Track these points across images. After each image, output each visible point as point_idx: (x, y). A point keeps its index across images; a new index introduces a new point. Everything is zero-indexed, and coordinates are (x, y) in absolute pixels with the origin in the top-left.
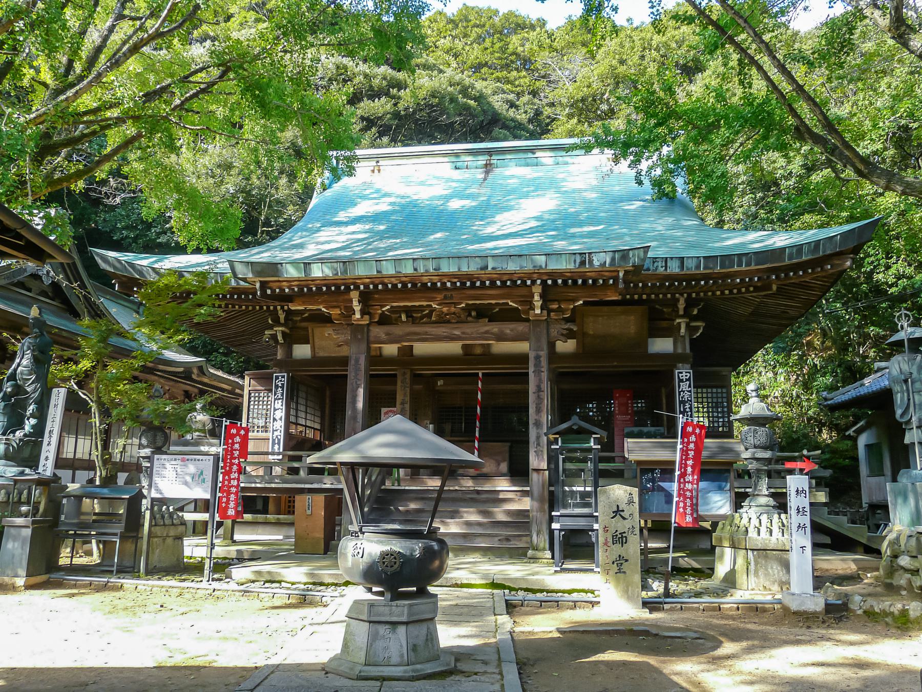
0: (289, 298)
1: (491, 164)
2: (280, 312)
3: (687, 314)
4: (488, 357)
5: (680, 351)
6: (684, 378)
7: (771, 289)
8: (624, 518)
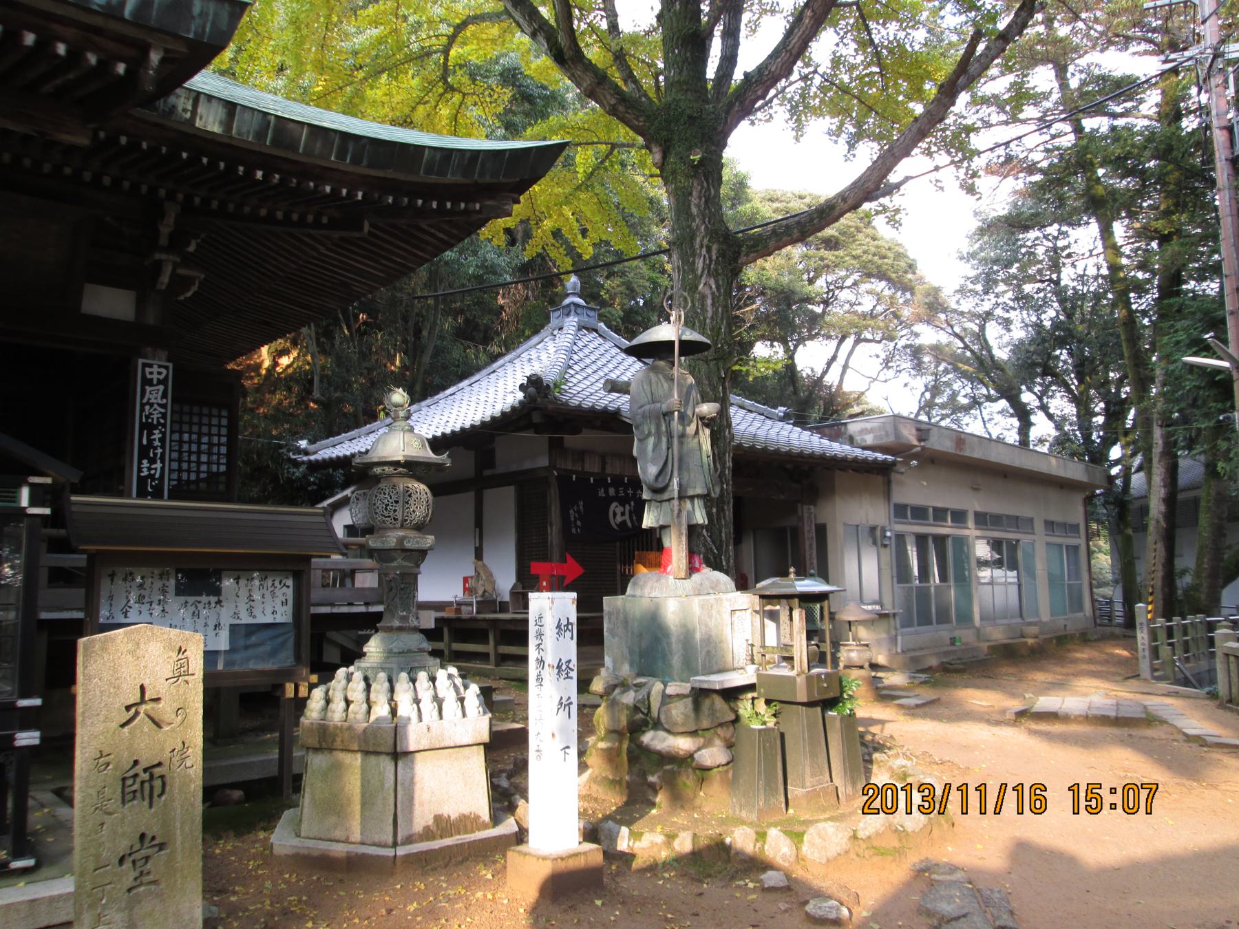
3: (177, 242)
5: (151, 318)
6: (155, 377)
7: (361, 229)
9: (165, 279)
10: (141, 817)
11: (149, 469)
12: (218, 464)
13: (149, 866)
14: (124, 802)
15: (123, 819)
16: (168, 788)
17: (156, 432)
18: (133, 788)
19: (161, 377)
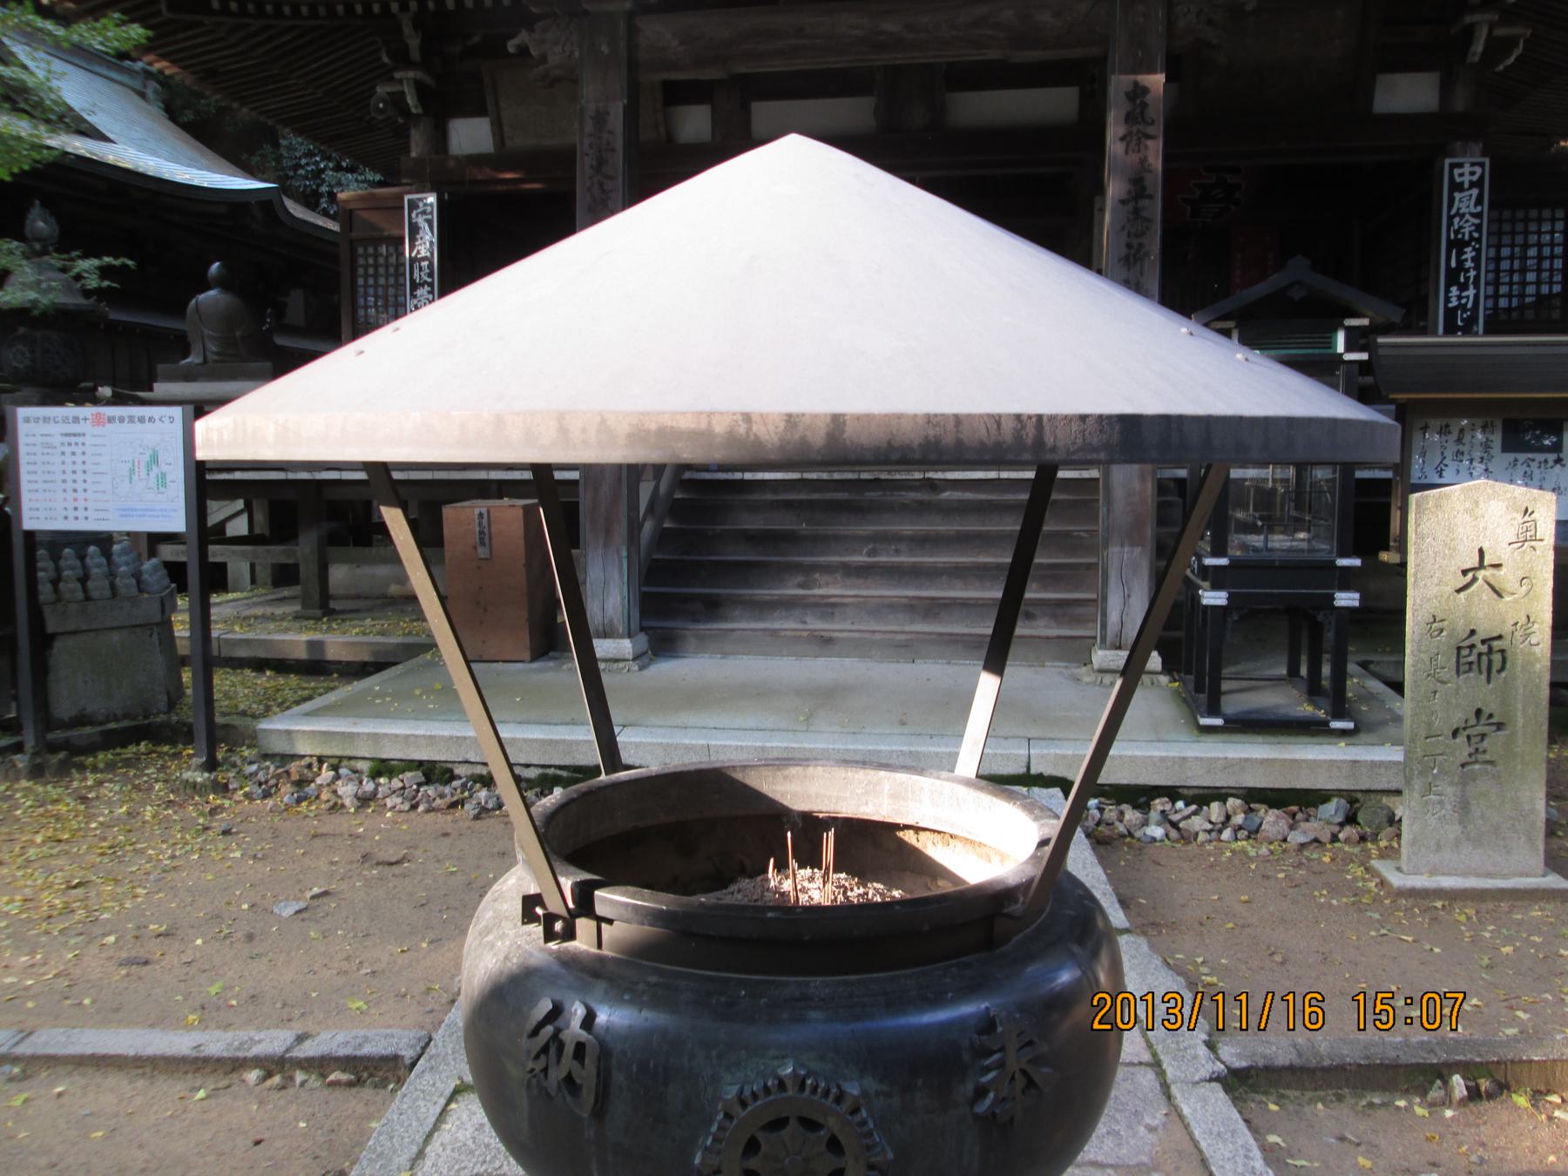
5: (1460, 104)
6: (1466, 179)
9: (1478, 47)
10: (1476, 691)
11: (1459, 298)
12: (1551, 283)
13: (1485, 744)
14: (1458, 673)
15: (1457, 691)
16: (1508, 665)
17: (1468, 250)
18: (1470, 659)
19: (1475, 178)
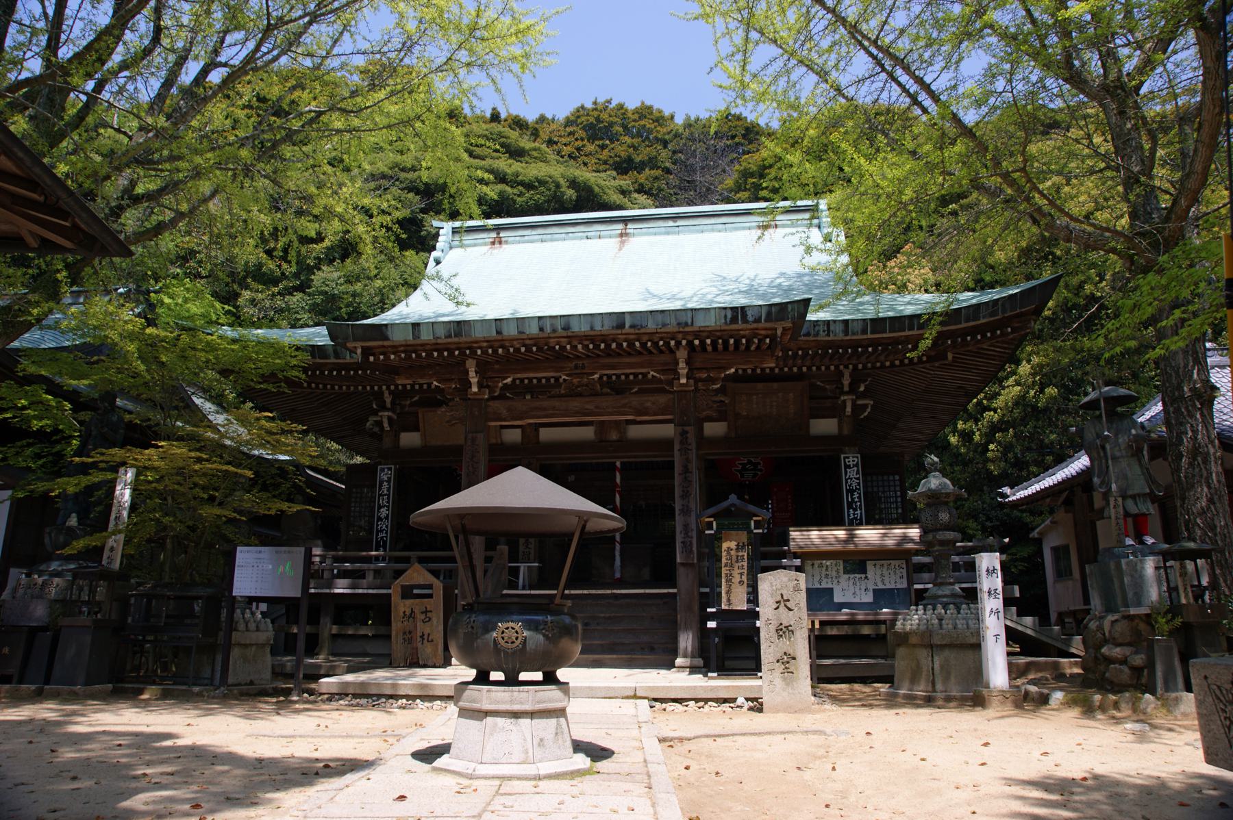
0: (393, 371)
1: (627, 234)
2: (386, 394)
3: (853, 389)
4: (626, 445)
5: (846, 432)
7: (946, 358)
8: (790, 610)
9: (849, 409)
